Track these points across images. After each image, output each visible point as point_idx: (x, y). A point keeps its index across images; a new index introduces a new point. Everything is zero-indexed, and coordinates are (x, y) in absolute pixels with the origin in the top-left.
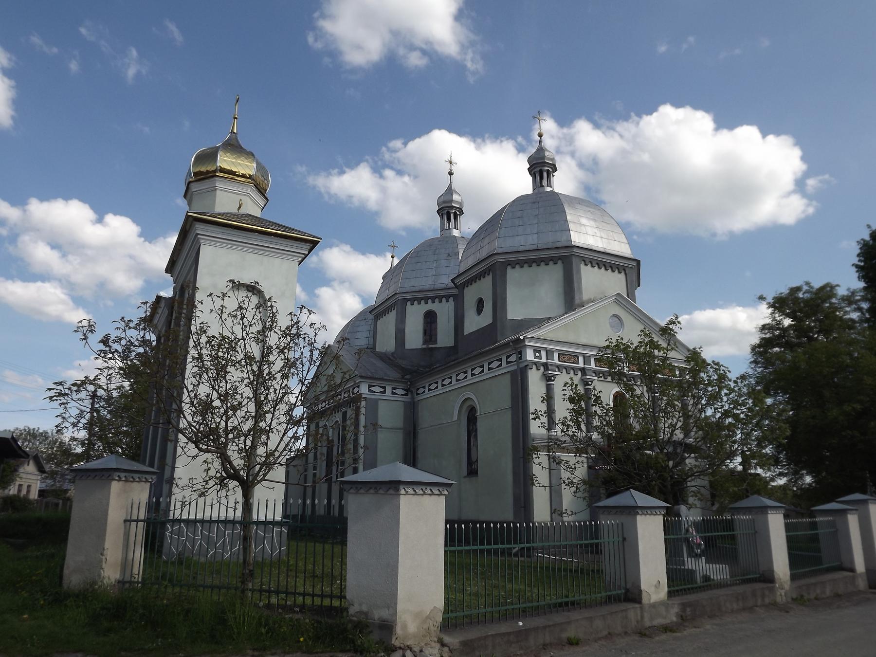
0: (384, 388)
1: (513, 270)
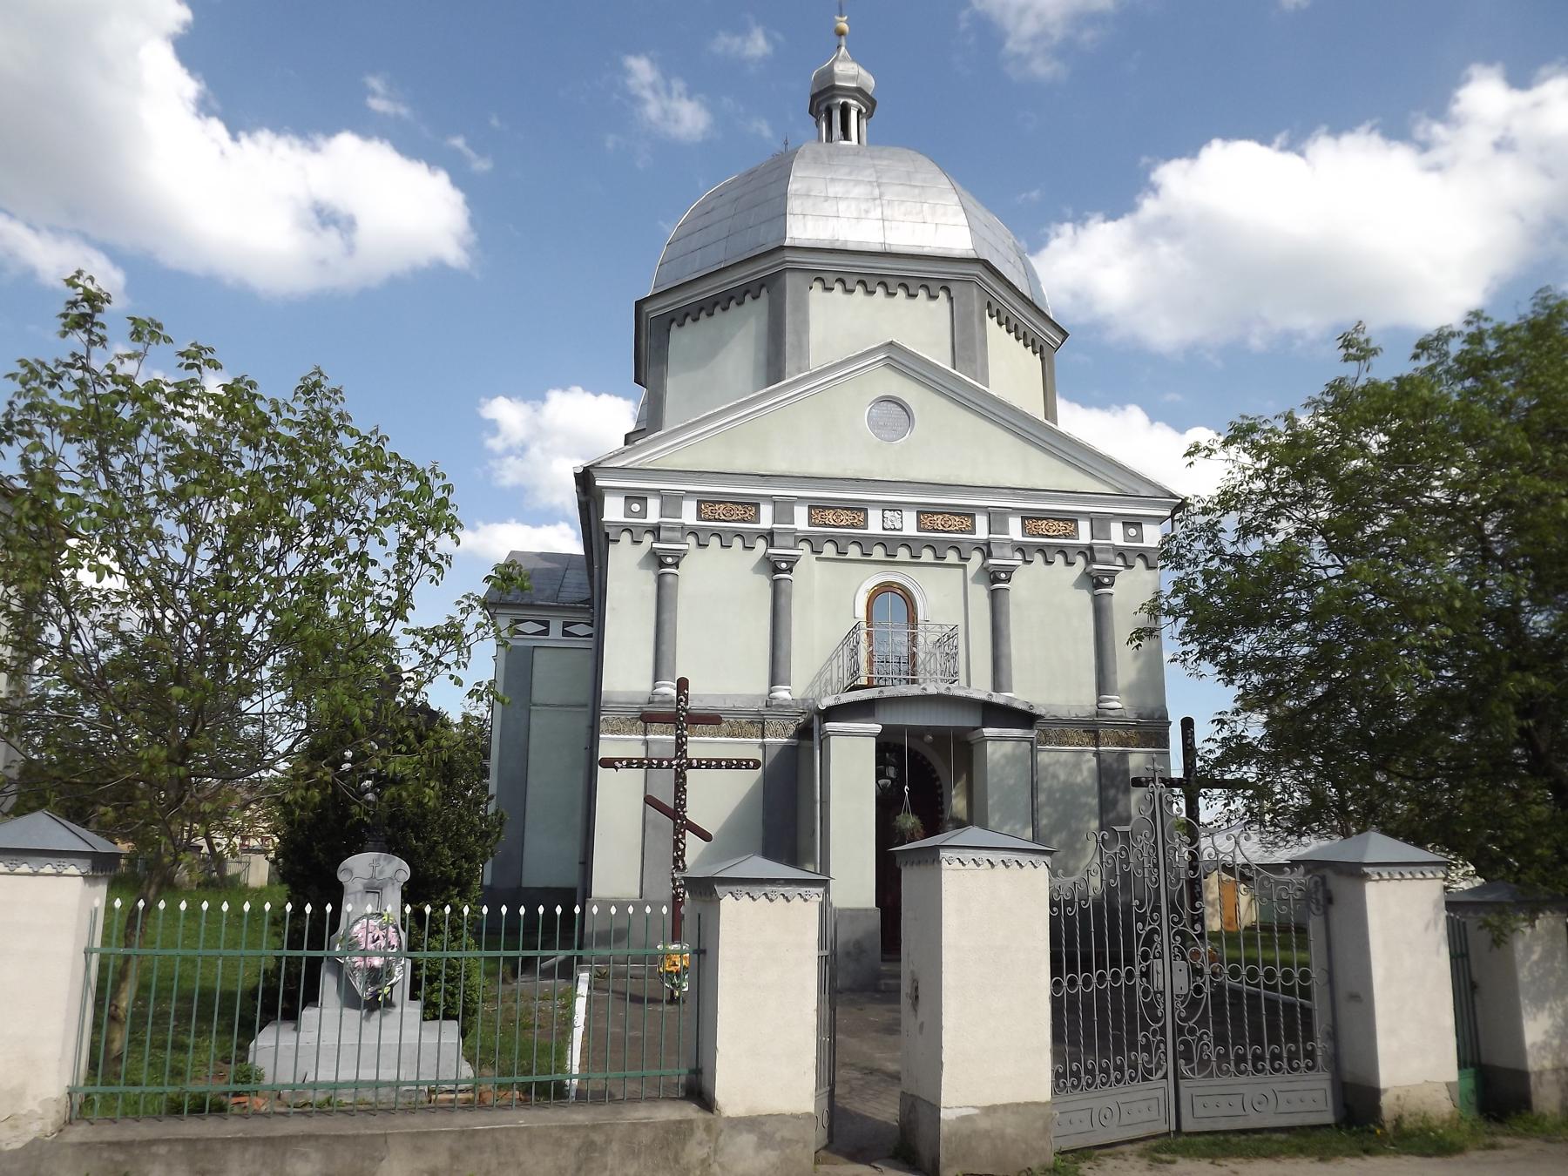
0: (546, 624)
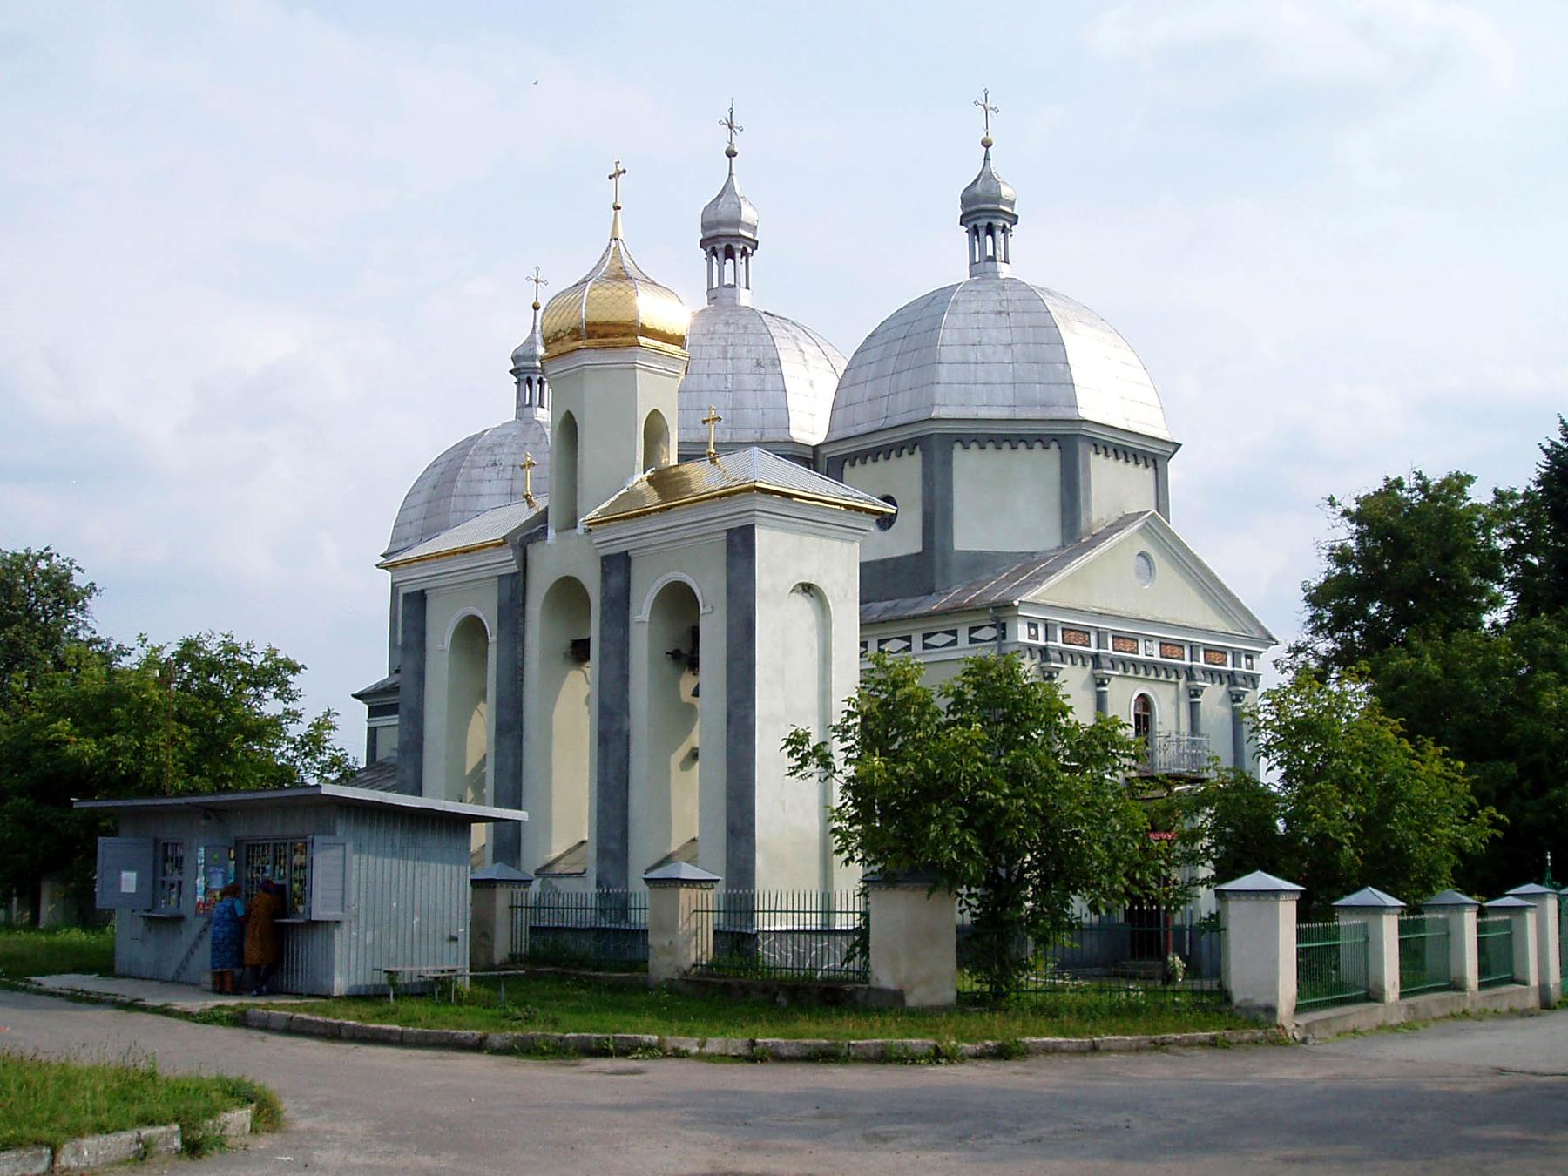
1: (966, 453)
